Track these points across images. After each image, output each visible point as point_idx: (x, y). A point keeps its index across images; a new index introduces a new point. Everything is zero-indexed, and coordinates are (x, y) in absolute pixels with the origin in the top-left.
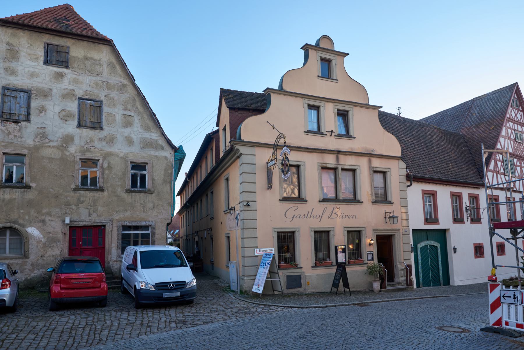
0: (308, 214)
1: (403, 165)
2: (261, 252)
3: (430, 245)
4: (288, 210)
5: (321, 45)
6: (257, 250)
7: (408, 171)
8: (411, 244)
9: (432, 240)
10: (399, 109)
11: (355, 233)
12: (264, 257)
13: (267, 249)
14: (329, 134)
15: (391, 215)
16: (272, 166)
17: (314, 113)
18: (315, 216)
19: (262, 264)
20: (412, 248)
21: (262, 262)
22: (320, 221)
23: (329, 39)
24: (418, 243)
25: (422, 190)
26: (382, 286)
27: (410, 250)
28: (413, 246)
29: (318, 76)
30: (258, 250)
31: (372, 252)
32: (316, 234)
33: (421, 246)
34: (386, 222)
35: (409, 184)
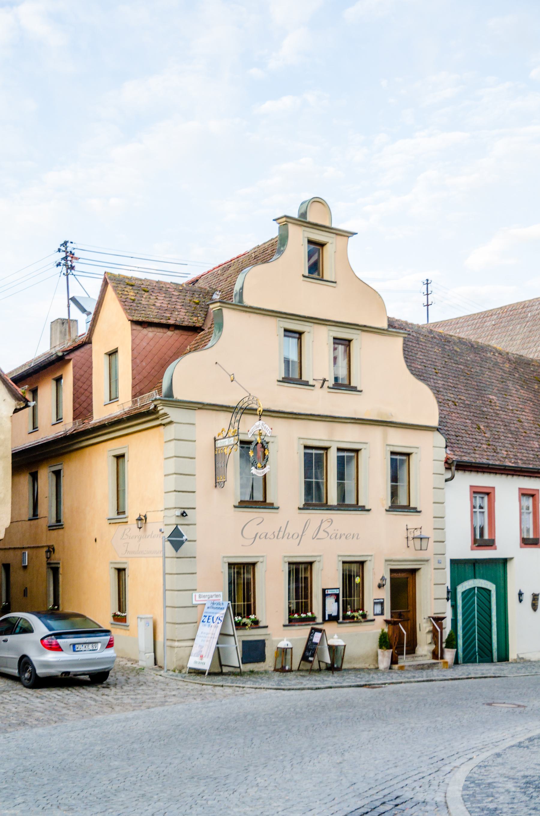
0: (279, 531)
1: (440, 440)
2: (201, 599)
3: (478, 588)
4: (246, 525)
5: (311, 218)
6: (195, 596)
7: (449, 452)
8: (446, 585)
9: (483, 578)
10: (427, 284)
11: (355, 564)
12: (208, 608)
13: (213, 594)
14: (318, 384)
15: (417, 534)
16: (228, 446)
17: (293, 342)
18: (291, 536)
19: (206, 620)
20: (448, 592)
21: (205, 616)
22: (299, 544)
23: (323, 204)
24: (458, 584)
25: (471, 487)
26: (394, 661)
27: (446, 597)
28: (450, 590)
29: (304, 276)
30: (197, 594)
31: (382, 600)
32: (292, 566)
33: (464, 590)
34: (408, 547)
35: (449, 475)
